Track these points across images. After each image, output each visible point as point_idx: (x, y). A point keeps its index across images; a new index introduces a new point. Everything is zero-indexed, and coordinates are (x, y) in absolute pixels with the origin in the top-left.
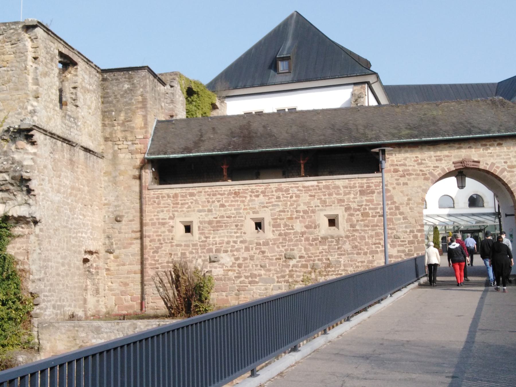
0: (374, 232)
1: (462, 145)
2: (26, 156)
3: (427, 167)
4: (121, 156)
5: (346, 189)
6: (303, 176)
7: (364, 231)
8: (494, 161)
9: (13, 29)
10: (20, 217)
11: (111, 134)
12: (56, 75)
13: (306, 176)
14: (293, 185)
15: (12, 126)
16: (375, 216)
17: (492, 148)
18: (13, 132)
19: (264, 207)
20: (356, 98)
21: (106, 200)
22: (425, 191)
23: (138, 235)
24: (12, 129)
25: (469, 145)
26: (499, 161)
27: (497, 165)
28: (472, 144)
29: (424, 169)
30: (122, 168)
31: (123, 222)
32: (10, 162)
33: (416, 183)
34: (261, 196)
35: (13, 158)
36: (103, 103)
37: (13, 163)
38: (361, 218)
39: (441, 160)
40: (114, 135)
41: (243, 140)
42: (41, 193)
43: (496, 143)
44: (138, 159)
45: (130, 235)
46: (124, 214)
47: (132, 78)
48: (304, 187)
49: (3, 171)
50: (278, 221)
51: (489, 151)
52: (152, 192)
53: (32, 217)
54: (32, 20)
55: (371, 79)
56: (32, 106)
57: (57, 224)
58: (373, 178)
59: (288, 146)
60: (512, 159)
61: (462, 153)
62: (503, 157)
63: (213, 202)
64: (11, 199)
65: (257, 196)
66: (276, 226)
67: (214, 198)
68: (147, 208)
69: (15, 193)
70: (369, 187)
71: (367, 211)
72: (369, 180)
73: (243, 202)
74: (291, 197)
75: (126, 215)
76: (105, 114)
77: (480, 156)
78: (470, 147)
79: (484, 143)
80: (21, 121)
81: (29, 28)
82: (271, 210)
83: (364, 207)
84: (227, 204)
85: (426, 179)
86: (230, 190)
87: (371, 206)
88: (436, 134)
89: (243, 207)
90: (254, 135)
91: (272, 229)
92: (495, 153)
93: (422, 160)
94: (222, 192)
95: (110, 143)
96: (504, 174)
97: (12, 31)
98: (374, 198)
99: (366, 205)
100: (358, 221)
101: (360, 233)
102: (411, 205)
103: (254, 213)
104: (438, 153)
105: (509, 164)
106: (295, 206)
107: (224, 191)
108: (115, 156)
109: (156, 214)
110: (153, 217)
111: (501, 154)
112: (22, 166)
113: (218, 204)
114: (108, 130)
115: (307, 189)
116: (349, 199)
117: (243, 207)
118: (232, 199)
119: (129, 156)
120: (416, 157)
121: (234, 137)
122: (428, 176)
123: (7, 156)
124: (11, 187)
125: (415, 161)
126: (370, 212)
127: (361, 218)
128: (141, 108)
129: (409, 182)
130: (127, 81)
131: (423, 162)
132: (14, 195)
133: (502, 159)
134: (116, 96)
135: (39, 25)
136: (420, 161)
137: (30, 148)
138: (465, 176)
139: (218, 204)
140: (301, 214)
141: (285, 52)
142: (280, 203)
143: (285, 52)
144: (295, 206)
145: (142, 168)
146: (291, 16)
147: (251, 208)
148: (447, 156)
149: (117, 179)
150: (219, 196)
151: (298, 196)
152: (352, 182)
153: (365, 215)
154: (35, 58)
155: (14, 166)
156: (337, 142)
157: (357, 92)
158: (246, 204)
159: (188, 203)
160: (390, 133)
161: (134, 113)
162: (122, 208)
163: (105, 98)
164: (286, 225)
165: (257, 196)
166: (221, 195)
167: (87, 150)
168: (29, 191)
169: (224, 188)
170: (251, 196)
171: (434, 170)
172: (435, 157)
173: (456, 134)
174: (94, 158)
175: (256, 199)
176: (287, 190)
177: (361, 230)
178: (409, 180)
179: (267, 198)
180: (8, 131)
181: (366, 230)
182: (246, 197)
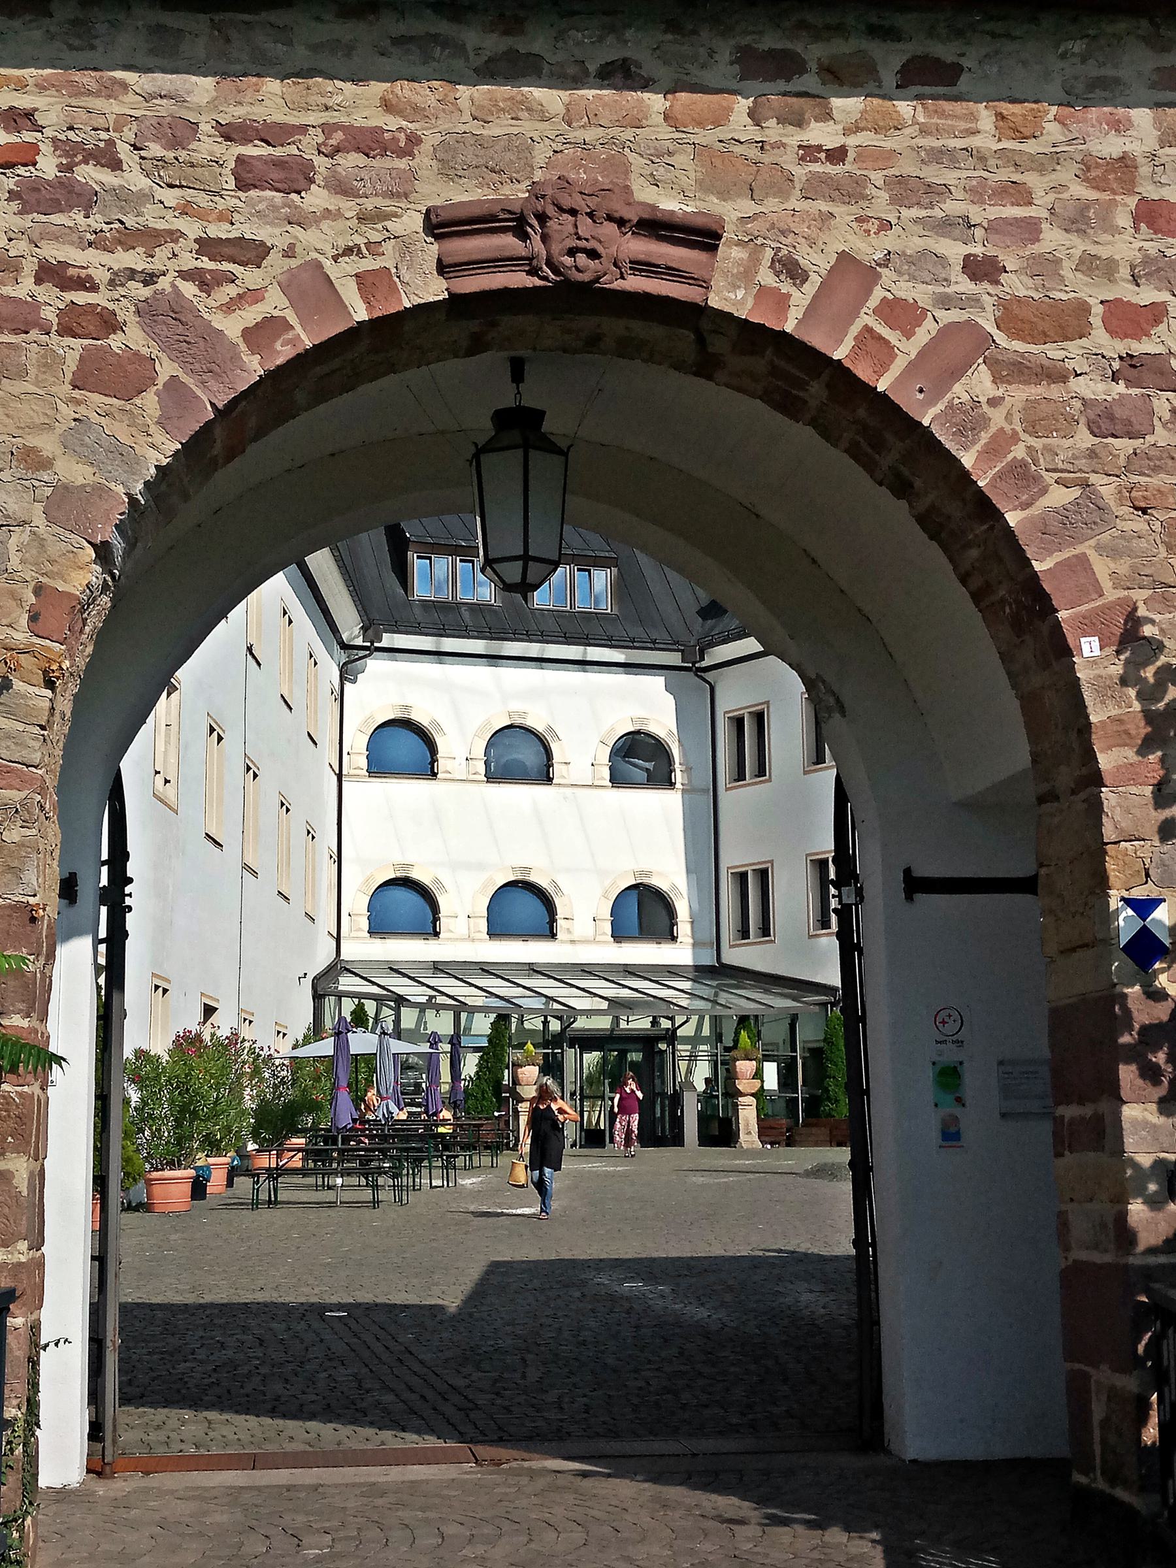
1: (538, 42)
3: (128, 238)
8: (870, 249)
17: (846, 106)
25: (610, 52)
29: (97, 264)
51: (822, 134)
60: (1052, 238)
62: (953, 207)
79: (770, 41)
92: (887, 157)
96: (959, 391)
105: (1016, 284)
111: (936, 175)
131: (89, 174)
136: (48, 166)
171: (206, 282)
172: (228, 133)
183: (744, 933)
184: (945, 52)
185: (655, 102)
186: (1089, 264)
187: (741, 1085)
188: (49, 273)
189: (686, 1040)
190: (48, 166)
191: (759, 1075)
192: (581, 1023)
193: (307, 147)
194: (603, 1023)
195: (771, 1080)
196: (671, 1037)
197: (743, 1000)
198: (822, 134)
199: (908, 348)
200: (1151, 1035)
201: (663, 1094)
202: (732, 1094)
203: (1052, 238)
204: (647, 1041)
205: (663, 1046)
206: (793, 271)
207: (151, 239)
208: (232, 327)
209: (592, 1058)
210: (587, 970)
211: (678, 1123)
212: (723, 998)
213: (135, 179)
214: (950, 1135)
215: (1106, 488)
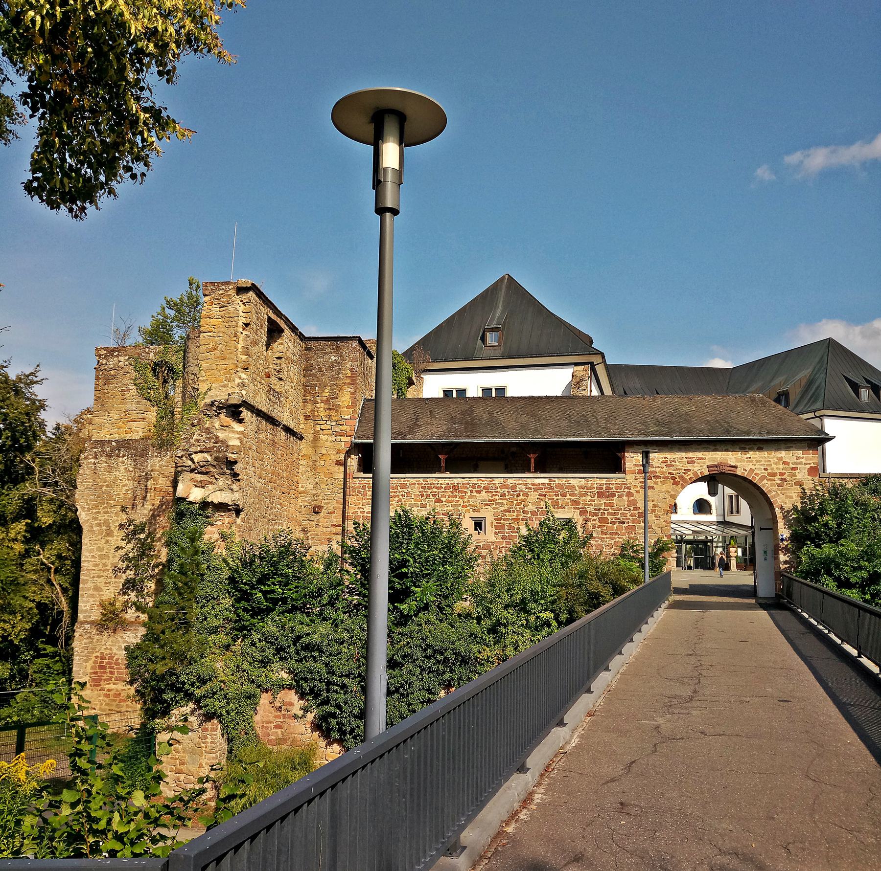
0: (613, 541)
1: (718, 447)
2: (231, 435)
3: (677, 469)
4: (324, 437)
5: (582, 490)
6: (533, 472)
7: (601, 538)
8: (753, 468)
9: (223, 289)
10: (220, 504)
11: (313, 411)
12: (264, 343)
13: (535, 472)
14: (520, 482)
15: (218, 399)
16: (615, 523)
17: (751, 453)
18: (218, 407)
19: (486, 505)
20: (577, 382)
21: (302, 487)
22: (674, 497)
23: (340, 529)
24: (216, 403)
25: (726, 448)
26: (759, 467)
27: (756, 471)
28: (728, 447)
29: (674, 472)
30: (324, 451)
31: (322, 514)
32: (213, 441)
33: (664, 488)
34: (483, 493)
35: (217, 437)
36: (304, 376)
37: (216, 442)
38: (599, 524)
39: (693, 462)
40: (316, 414)
41: (465, 427)
42: (245, 478)
43: (756, 447)
44: (345, 443)
45: (329, 530)
46: (323, 505)
47: (341, 349)
48: (533, 484)
49: (205, 450)
50: (502, 521)
51: (748, 455)
52: (357, 481)
53: (235, 505)
54: (245, 281)
55: (596, 359)
56: (240, 377)
57: (257, 513)
58: (614, 478)
59: (517, 437)
60: (773, 466)
61: (717, 456)
62: (762, 463)
63: (428, 496)
64: (211, 483)
65: (479, 492)
66: (499, 527)
67: (429, 491)
68: (350, 500)
69: (217, 476)
70: (608, 488)
71: (606, 516)
72: (609, 481)
73: (462, 497)
74: (518, 495)
75: (326, 506)
76: (307, 388)
77: (738, 460)
78: (727, 450)
79: (743, 446)
80: (229, 395)
81: (241, 290)
82: (494, 509)
83: (602, 511)
84: (444, 499)
85: (676, 483)
86: (448, 484)
87: (610, 511)
88: (690, 433)
89: (462, 504)
90: (478, 422)
91: (494, 530)
92: (755, 458)
93: (672, 461)
94: (439, 485)
95: (311, 422)
96: (763, 482)
97: (221, 292)
98: (614, 502)
99: (604, 510)
100: (594, 527)
101: (596, 541)
102: (657, 513)
103: (474, 511)
104: (691, 455)
105: (769, 471)
106: (522, 506)
107: (441, 484)
108: (316, 438)
109: (360, 506)
110: (357, 510)
111: (761, 459)
112: (227, 446)
113: (433, 499)
114: (310, 407)
115: (537, 487)
116: (584, 501)
117: (462, 504)
118: (450, 493)
119: (333, 438)
120: (665, 458)
121: (455, 424)
122: (678, 479)
123: (209, 433)
124: (212, 469)
125: (663, 462)
126: (609, 517)
127: (599, 524)
128: (349, 384)
129: (655, 486)
130: (334, 352)
131: (673, 463)
132: (216, 479)
133: (761, 465)
134: (320, 368)
135: (254, 288)
136: (669, 463)
137: (238, 427)
138: (718, 482)
139: (433, 499)
140: (529, 515)
141: (495, 323)
142: (505, 502)
143: (495, 323)
144: (522, 506)
145: (348, 454)
146: (502, 279)
147: (471, 506)
148: (701, 459)
149: (318, 464)
150: (435, 490)
151: (526, 495)
152: (590, 482)
153: (603, 520)
154: (247, 325)
155: (217, 445)
156: (574, 436)
157: (579, 374)
158: (466, 500)
159: (398, 496)
160: (636, 429)
161: (341, 389)
162: (321, 497)
163: (307, 371)
164: (510, 527)
165: (479, 492)
166: (437, 488)
167: (287, 430)
168: (235, 475)
169: (441, 481)
170: (471, 491)
171: (685, 473)
172: (686, 458)
173: (711, 434)
174: (293, 439)
175: (478, 495)
176: (514, 487)
177: (598, 538)
178: (655, 483)
179: (490, 495)
180: (212, 404)
181: (604, 538)
182: (466, 493)
183: (732, 513)
184: (761, 446)
185: (730, 453)
186: (777, 468)
187: (731, 554)
188: (669, 473)
189: (715, 542)
190: (669, 463)
191: (736, 552)
192: (687, 537)
193: (694, 459)
194: (691, 537)
195: (740, 553)
196: (712, 541)
197: (733, 532)
198: (748, 455)
199: (758, 478)
200: (783, 548)
201: (710, 557)
202: (728, 556)
203: (773, 466)
204: (705, 542)
205: (709, 544)
206: (746, 470)
207: (680, 469)
208: (688, 478)
209: (688, 546)
210: (686, 522)
211: (714, 564)
212: (726, 531)
213: (677, 463)
214: (765, 559)
215: (779, 492)
